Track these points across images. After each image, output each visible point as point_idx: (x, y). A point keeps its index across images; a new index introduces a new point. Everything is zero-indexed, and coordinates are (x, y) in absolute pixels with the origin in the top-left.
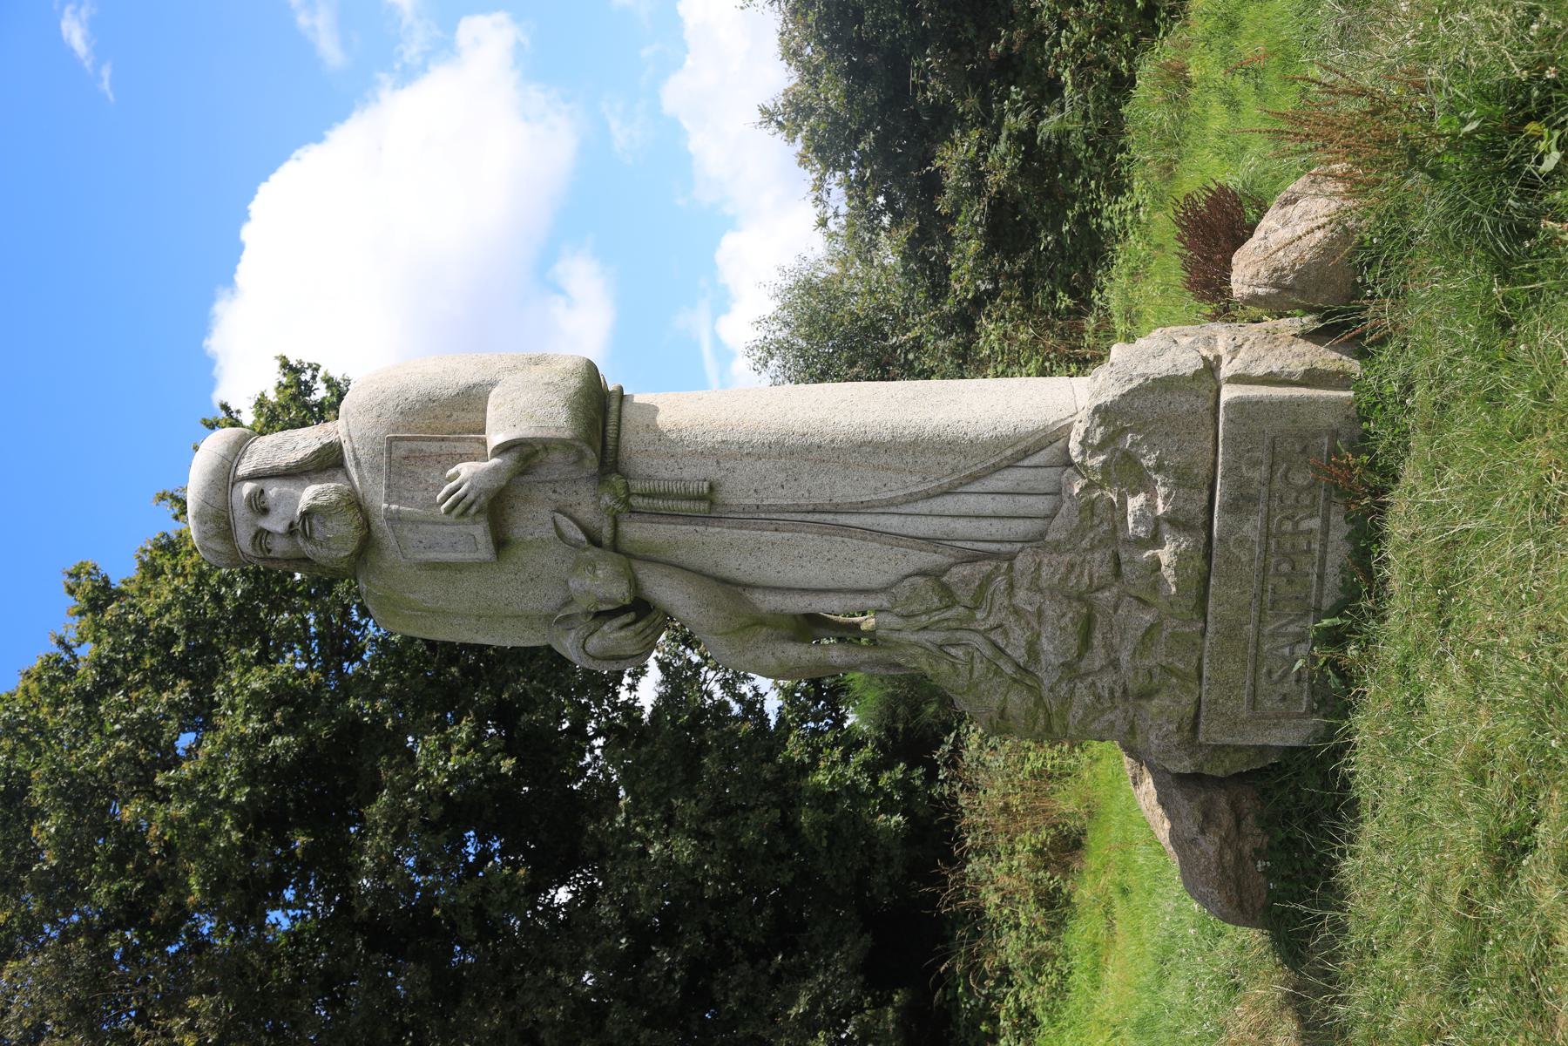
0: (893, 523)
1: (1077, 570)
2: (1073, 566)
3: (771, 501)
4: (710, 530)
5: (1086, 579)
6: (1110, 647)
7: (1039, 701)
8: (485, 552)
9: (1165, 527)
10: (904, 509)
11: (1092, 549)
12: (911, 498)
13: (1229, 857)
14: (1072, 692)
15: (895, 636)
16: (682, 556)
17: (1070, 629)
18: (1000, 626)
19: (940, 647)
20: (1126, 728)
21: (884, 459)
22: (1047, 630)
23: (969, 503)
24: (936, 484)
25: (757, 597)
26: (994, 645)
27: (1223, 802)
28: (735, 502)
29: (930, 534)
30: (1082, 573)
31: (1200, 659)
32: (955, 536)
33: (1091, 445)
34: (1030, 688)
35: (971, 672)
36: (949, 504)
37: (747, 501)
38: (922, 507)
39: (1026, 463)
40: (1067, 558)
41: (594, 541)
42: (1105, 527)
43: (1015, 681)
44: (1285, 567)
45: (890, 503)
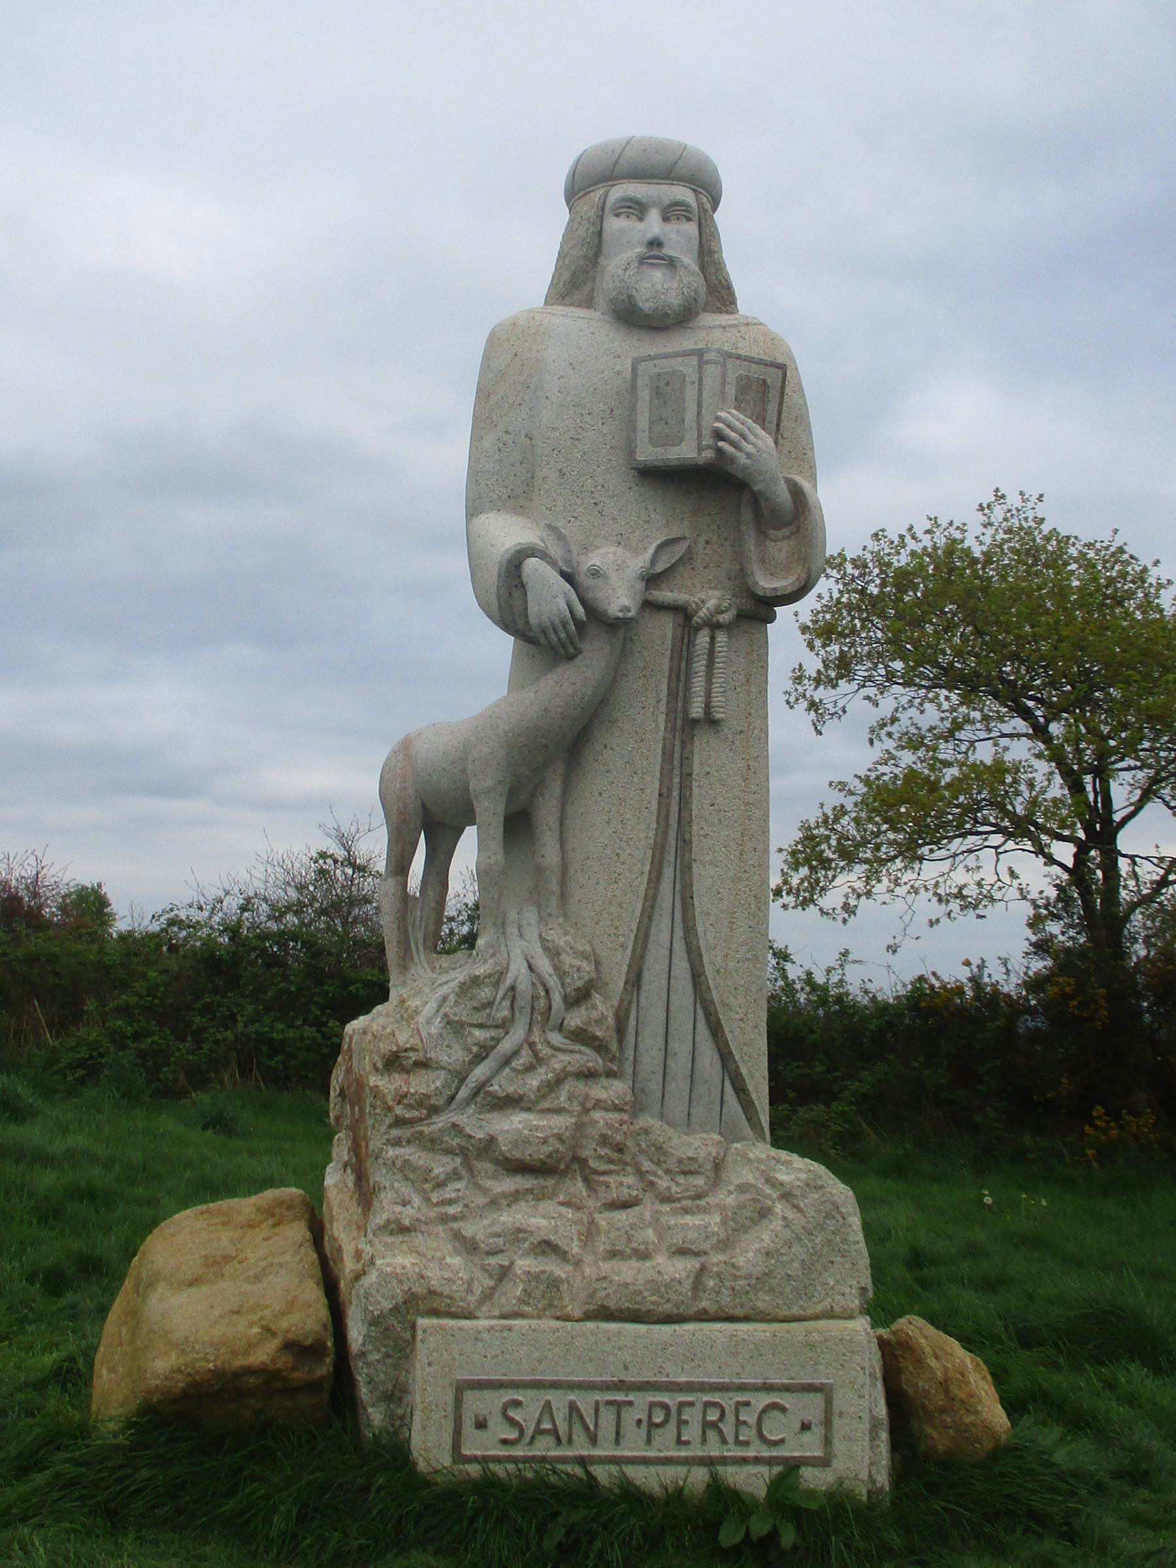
0: (661, 932)
1: (615, 1156)
3: (696, 791)
4: (662, 718)
5: (604, 1167)
7: (434, 1110)
8: (647, 454)
10: (679, 947)
11: (641, 1174)
14: (450, 1152)
19: (513, 988)
22: (533, 1119)
24: (712, 986)
26: (515, 1054)
28: (696, 750)
29: (646, 976)
30: (611, 1161)
32: (642, 1012)
35: (480, 1026)
36: (684, 997)
37: (696, 762)
38: (682, 967)
43: (462, 1080)
45: (689, 931)
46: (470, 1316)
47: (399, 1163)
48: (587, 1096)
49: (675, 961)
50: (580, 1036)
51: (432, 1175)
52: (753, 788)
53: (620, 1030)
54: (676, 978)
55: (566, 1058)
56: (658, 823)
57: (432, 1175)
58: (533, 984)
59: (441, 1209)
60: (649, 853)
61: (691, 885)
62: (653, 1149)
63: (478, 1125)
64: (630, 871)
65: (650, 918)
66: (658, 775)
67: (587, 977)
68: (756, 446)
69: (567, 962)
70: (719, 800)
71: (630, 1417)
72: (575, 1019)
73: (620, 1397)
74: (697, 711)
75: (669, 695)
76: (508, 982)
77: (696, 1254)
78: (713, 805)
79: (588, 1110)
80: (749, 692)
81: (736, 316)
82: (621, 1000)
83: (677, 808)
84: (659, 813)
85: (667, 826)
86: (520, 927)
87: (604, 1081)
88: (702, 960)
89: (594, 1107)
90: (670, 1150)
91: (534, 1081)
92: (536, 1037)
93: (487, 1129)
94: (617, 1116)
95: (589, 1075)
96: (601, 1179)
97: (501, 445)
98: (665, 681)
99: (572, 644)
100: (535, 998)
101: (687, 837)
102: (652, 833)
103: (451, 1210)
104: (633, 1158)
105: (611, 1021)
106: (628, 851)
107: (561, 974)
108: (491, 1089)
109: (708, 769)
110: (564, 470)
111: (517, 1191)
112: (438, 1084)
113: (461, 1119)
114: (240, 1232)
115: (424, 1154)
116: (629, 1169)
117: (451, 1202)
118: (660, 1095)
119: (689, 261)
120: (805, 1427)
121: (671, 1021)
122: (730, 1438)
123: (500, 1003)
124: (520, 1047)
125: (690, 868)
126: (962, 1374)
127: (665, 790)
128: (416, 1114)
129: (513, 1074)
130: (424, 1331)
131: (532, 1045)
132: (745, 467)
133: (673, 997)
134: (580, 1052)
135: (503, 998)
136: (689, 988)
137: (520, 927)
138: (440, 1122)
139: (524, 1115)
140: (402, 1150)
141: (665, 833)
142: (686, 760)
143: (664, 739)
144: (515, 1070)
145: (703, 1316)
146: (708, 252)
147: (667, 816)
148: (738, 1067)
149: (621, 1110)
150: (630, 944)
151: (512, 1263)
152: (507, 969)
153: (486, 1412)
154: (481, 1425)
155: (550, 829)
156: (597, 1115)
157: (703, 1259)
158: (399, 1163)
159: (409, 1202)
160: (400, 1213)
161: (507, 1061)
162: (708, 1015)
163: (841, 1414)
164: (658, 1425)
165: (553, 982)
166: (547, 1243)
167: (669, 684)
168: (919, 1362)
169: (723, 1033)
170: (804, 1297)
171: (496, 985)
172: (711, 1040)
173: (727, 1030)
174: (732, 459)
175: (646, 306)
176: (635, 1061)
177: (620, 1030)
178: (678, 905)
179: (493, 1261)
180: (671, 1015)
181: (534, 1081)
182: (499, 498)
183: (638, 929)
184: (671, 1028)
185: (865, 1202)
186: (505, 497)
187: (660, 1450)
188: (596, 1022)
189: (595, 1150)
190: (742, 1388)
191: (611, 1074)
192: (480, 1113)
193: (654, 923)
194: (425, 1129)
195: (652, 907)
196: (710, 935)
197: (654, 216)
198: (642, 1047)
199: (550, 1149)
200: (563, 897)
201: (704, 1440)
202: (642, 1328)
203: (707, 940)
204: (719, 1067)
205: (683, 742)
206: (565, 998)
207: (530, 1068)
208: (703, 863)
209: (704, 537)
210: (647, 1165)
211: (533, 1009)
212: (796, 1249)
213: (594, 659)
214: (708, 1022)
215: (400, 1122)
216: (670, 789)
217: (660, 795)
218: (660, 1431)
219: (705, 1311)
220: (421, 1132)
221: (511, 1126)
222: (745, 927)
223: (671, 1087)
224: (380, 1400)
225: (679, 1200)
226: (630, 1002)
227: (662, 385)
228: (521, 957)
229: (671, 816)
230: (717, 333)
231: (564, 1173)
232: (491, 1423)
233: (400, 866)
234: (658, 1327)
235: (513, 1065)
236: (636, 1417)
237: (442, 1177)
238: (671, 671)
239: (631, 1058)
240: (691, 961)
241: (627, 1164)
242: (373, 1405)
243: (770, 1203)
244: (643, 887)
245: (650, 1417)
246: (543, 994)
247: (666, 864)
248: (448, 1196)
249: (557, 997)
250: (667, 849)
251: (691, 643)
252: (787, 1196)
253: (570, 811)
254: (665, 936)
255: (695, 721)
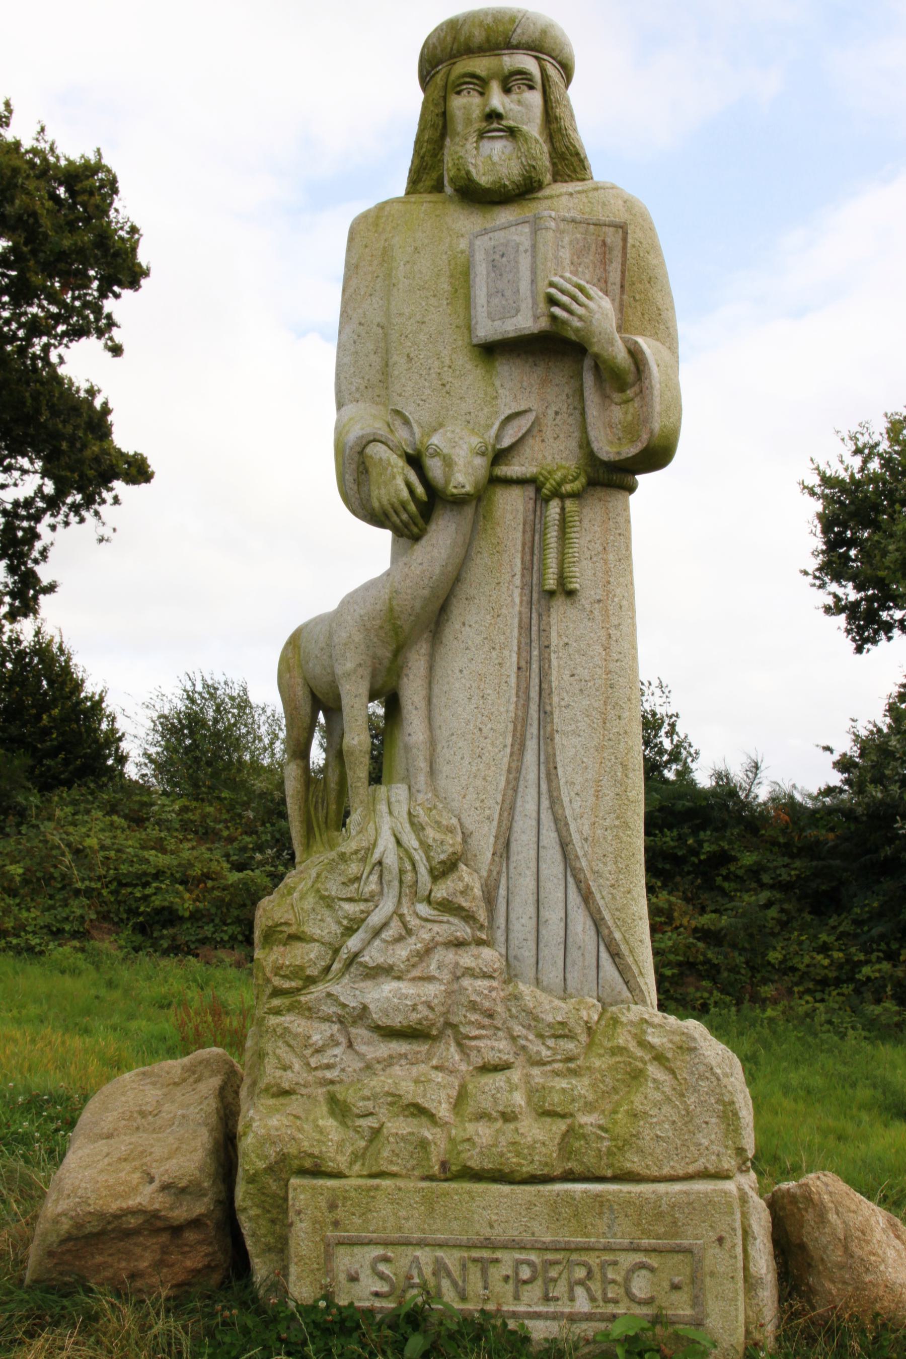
0: (527, 804)
1: (486, 1021)
2: (491, 1016)
3: (554, 663)
4: (517, 592)
5: (475, 1032)
6: (390, 1061)
7: (311, 981)
8: (488, 329)
9: (562, 1126)
10: (546, 817)
11: (514, 1039)
12: (560, 824)
13: (133, 1222)
14: (327, 1019)
15: (383, 808)
16: (481, 561)
17: (414, 1016)
18: (409, 932)
19: (380, 863)
20: (286, 1086)
21: (609, 793)
22: (405, 987)
23: (554, 891)
24: (580, 853)
25: (423, 648)
26: (385, 925)
27: (200, 1208)
28: (553, 621)
30: (483, 1027)
31: (394, 1175)
33: (644, 1032)
34: (328, 969)
35: (350, 900)
36: (553, 867)
37: (554, 635)
38: (550, 837)
39: (604, 955)
40: (500, 1009)
41: (499, 456)
42: (545, 1053)
43: (336, 951)
44: (525, 1273)
45: (555, 802)
46: (339, 1175)
47: (279, 1031)
48: (457, 964)
49: (543, 831)
50: (447, 907)
51: (311, 1042)
52: (615, 656)
53: (490, 900)
54: (544, 847)
55: (436, 928)
56: (518, 696)
57: (311, 1042)
58: (401, 858)
59: (319, 1074)
60: (511, 727)
61: (555, 754)
62: (524, 1014)
63: (348, 991)
64: (493, 744)
65: (515, 790)
66: (515, 649)
67: (451, 850)
68: (600, 313)
69: (431, 836)
70: (579, 670)
71: (497, 1273)
72: (441, 892)
73: (486, 1254)
74: (551, 583)
75: (523, 569)
76: (376, 856)
77: (563, 1116)
78: (573, 675)
79: (458, 978)
80: (606, 562)
81: (588, 184)
82: (490, 871)
83: (537, 681)
84: (518, 686)
85: (528, 698)
86: (389, 804)
87: (474, 950)
88: (568, 830)
89: (463, 975)
90: (541, 1015)
91: (402, 952)
92: (405, 910)
93: (360, 999)
94: (486, 983)
95: (459, 944)
96: (473, 1043)
97: (356, 337)
98: (519, 555)
99: (416, 524)
100: (402, 872)
101: (548, 708)
102: (512, 707)
103: (329, 1075)
104: (504, 1023)
105: (477, 892)
106: (489, 726)
107: (426, 847)
108: (362, 959)
109: (566, 640)
110: (412, 355)
111: (391, 1057)
112: (312, 956)
113: (335, 989)
114: (165, 1090)
115: (303, 1022)
116: (500, 1034)
117: (329, 1067)
118: (534, 960)
119: (533, 128)
120: (676, 1287)
121: (541, 890)
122: (599, 1295)
123: (368, 877)
124: (391, 918)
125: (552, 740)
126: (863, 1233)
127: (523, 664)
128: (294, 984)
129: (383, 945)
130: (295, 1189)
131: (401, 916)
132: (577, 331)
133: (543, 866)
134: (448, 922)
135: (370, 873)
136: (558, 857)
137: (389, 804)
138: (318, 991)
139: (395, 984)
140: (283, 1018)
141: (526, 706)
142: (544, 631)
143: (520, 613)
144: (385, 941)
145: (569, 1177)
146: (554, 122)
147: (528, 688)
148: (611, 932)
149: (491, 977)
150: (496, 816)
151: (382, 1125)
152: (375, 845)
153: (357, 1266)
154: (353, 1279)
155: (416, 708)
156: (466, 982)
157: (569, 1121)
158: (279, 1031)
159: (290, 1067)
160: (281, 1077)
161: (377, 933)
162: (578, 882)
163: (712, 1274)
164: (525, 1282)
165: (419, 857)
166: (416, 1106)
167: (522, 558)
168: (822, 1218)
169: (595, 900)
170: (676, 1158)
171: (364, 860)
172: (583, 906)
173: (598, 896)
174: (564, 323)
175: (484, 180)
176: (507, 929)
177: (490, 900)
178: (543, 776)
179: (364, 1123)
180: (541, 884)
181: (402, 952)
182: (357, 389)
183: (503, 801)
184: (542, 895)
185: (749, 1061)
186: (362, 387)
187: (530, 1306)
188: (462, 892)
189: (465, 1016)
190: (608, 1249)
191: (480, 943)
192: (354, 982)
193: (520, 795)
194: (302, 998)
195: (517, 779)
196: (576, 805)
197: (495, 87)
198: (513, 916)
199: (419, 1016)
200: (432, 772)
201: (572, 1299)
202: (506, 1189)
203: (573, 810)
204: (592, 933)
205: (540, 615)
206: (431, 871)
207: (399, 939)
208: (565, 734)
209: (554, 408)
210: (518, 1030)
211: (401, 882)
212: (666, 1109)
213: (443, 536)
214: (579, 889)
215: (277, 992)
216: (529, 662)
217: (519, 668)
218: (528, 1287)
219: (571, 1172)
220: (299, 1002)
221: (382, 996)
222: (612, 795)
223: (544, 952)
224: (264, 1251)
225: (549, 1063)
226: (499, 873)
227: (497, 257)
228: (389, 832)
229: (532, 689)
230: (564, 199)
231: (435, 1039)
232: (362, 1277)
233: (301, 752)
234: (522, 1187)
235: (383, 936)
236: (504, 1273)
237: (320, 1043)
238: (524, 544)
239: (503, 926)
240: (558, 830)
241: (498, 1029)
242: (258, 1256)
243: (640, 1065)
244: (506, 760)
245: (517, 1274)
246: (409, 868)
247: (528, 736)
248: (326, 1061)
249: (423, 870)
250: (529, 721)
251: (543, 516)
252: (659, 1058)
253: (436, 690)
254: (531, 807)
255: (552, 593)
